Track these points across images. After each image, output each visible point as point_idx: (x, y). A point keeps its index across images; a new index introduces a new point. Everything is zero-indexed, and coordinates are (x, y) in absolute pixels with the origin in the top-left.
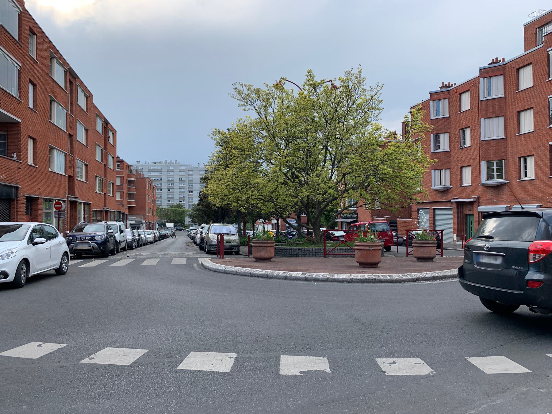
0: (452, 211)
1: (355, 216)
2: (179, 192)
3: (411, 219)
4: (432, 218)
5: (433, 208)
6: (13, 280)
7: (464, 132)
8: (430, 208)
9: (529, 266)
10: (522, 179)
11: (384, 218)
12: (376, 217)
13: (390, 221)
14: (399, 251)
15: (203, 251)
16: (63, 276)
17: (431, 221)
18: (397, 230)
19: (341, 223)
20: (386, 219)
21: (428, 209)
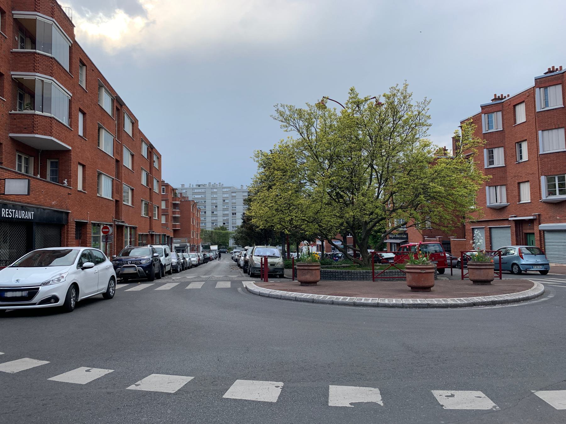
1: (405, 236)
3: (465, 239)
4: (488, 238)
5: (489, 227)
8: (485, 227)
11: (436, 238)
17: (487, 241)
20: (438, 239)
21: (484, 228)
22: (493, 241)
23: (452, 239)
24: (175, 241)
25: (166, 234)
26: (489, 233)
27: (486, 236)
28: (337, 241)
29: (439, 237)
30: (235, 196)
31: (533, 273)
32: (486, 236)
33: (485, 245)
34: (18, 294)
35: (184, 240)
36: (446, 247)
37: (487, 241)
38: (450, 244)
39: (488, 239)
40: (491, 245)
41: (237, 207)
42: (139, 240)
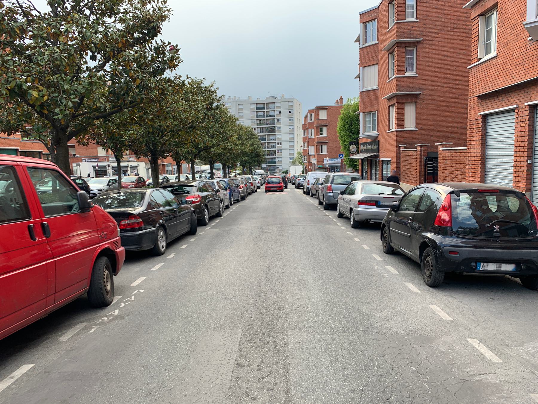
0: (514, 124)
1: (375, 147)
2: (289, 138)
3: (466, 148)
4: (523, 139)
5: (530, 105)
6: (518, 208)
7: (322, 129)
8: (517, 108)
9: (46, 302)
10: (391, 131)
11: (416, 147)
12: (405, 148)
13: (428, 154)
14: (115, 285)
15: (310, 196)
16: (161, 256)
17: (519, 149)
18: (376, 201)
19: (361, 161)
20: (418, 149)
21: (512, 110)
22: (489, 131)
23: (441, 149)
24: (112, 159)
25: (42, 152)
26: (529, 125)
27: (519, 134)
28: (332, 159)
29: (420, 146)
30: (242, 109)
31: (495, 101)
32: (519, 134)
33: (512, 161)
34: (276, 189)
35: (126, 158)
36: (432, 167)
37: (519, 149)
38: (437, 159)
39: (522, 144)
40: (529, 162)
41: (244, 121)
42: (305, 160)
